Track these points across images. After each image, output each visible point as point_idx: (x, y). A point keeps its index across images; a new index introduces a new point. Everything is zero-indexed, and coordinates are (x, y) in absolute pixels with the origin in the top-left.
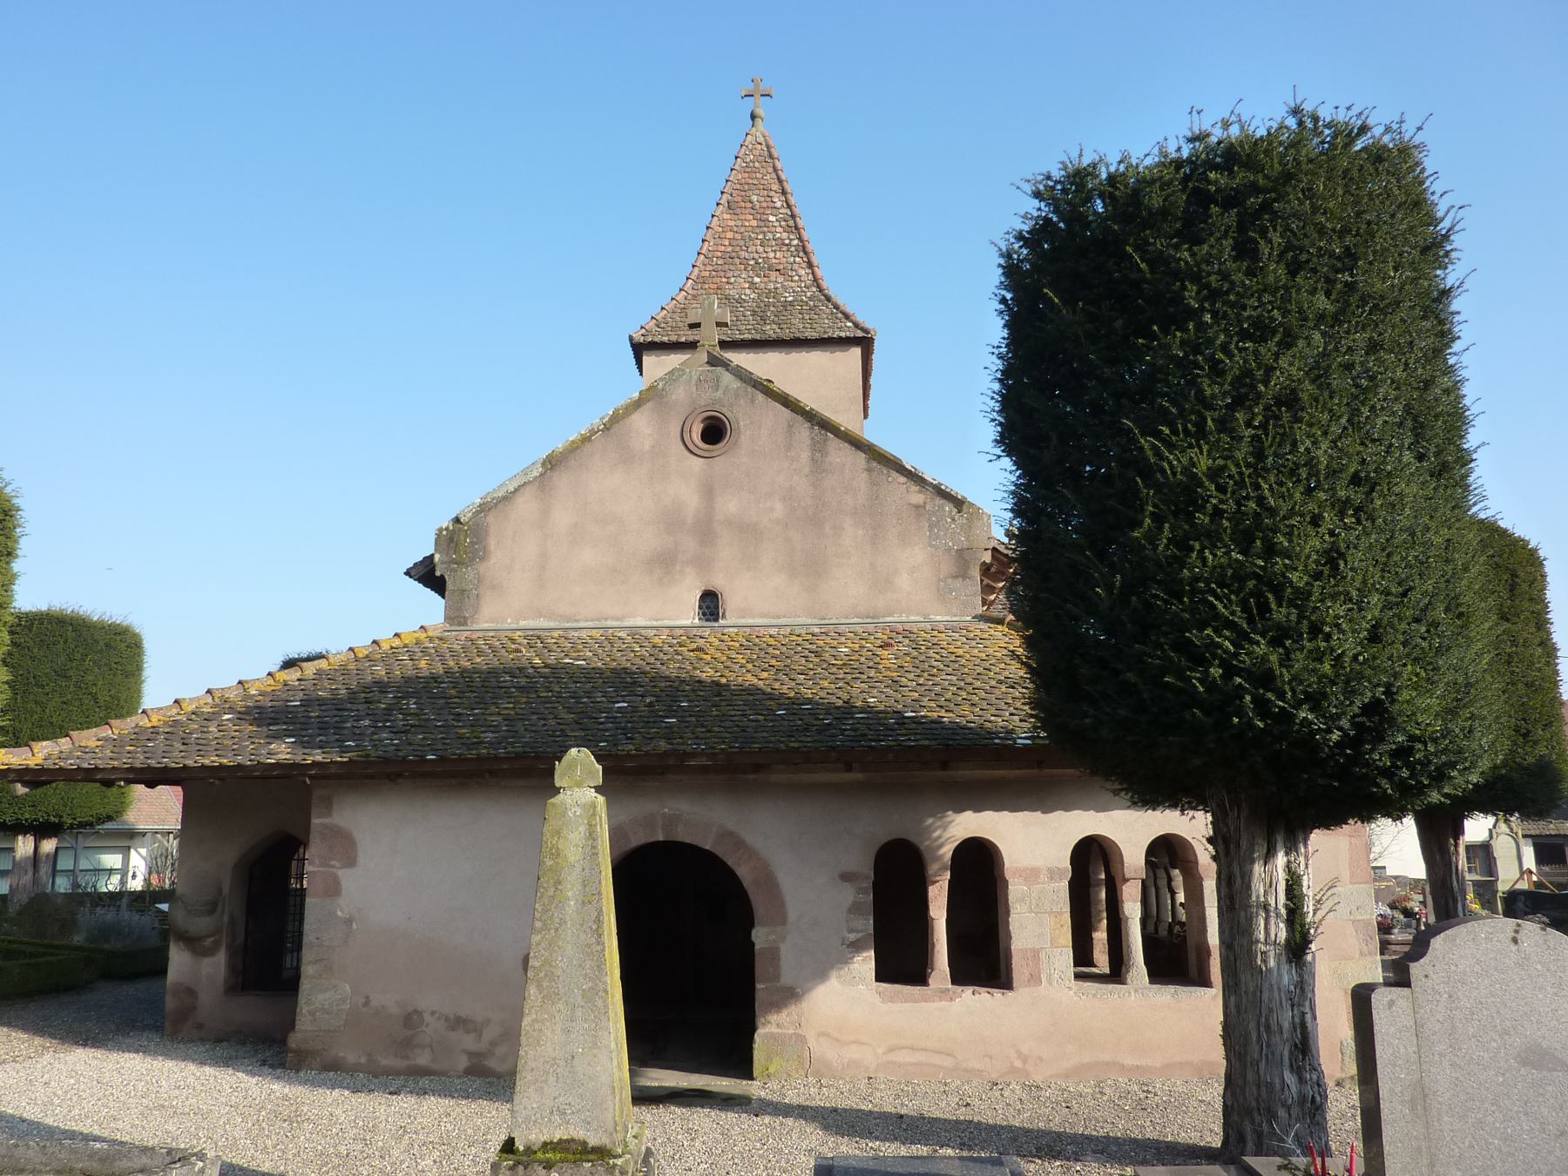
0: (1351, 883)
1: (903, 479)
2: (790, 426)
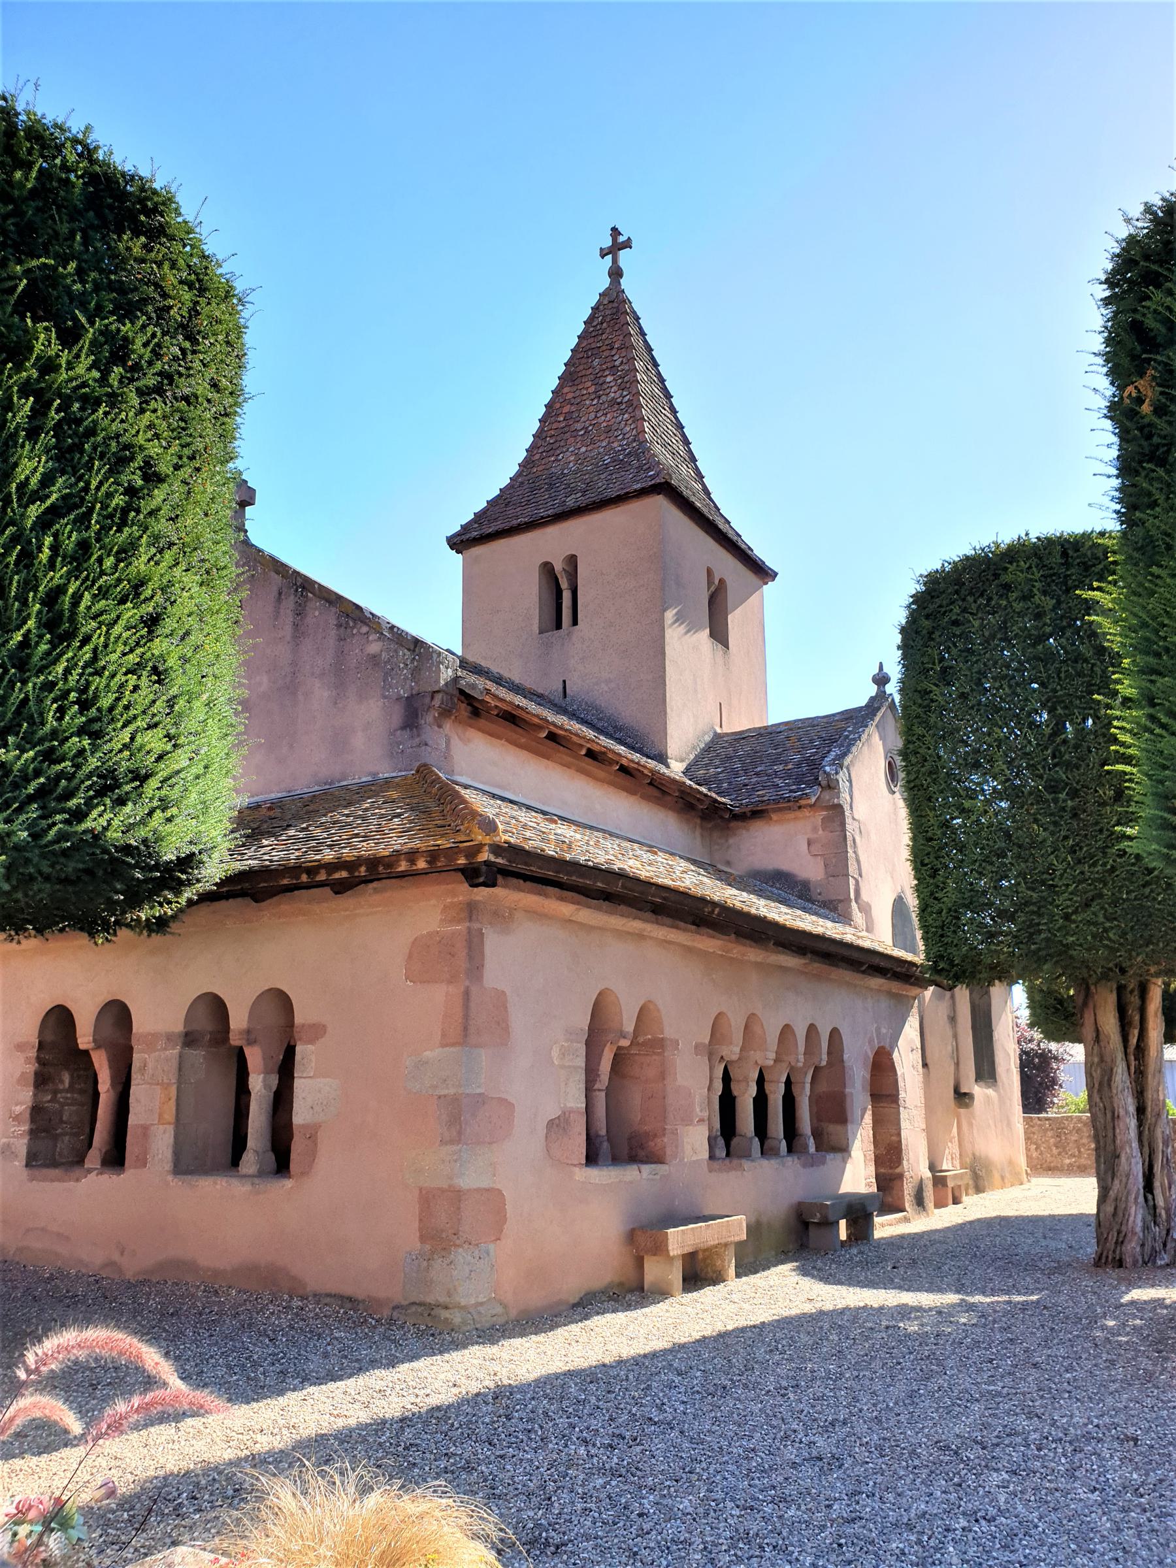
0: (443, 1045)
2: (280, 594)
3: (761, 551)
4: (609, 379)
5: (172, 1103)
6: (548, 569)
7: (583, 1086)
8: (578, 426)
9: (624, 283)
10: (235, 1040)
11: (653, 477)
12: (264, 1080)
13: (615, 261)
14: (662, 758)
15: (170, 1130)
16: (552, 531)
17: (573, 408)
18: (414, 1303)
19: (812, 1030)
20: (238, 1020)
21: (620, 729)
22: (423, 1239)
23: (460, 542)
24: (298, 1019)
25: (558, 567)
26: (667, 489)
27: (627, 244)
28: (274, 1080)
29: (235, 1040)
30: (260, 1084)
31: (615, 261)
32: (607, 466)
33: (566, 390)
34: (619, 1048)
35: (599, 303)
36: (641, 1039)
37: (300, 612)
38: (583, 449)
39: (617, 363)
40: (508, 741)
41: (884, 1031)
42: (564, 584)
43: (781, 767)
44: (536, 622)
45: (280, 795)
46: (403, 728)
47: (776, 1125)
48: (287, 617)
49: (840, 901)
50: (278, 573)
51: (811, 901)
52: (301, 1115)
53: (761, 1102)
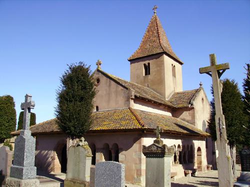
3: (182, 62)
19: (188, 146)
47: (182, 160)
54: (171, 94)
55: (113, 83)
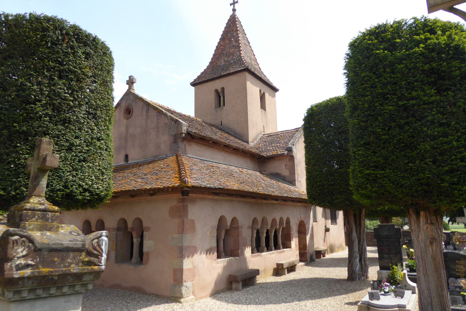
1: (164, 116)
2: (143, 107)
3: (275, 84)
4: (233, 39)
5: (114, 246)
6: (217, 91)
7: (216, 240)
8: (225, 52)
9: (237, 13)
10: (129, 230)
11: (244, 67)
12: (137, 240)
13: (234, 7)
14: (247, 142)
15: (114, 252)
16: (218, 81)
17: (223, 47)
18: (172, 297)
19: (281, 220)
20: (130, 225)
21: (237, 134)
22: (174, 281)
23: (193, 84)
24: (144, 225)
25: (220, 90)
26: (247, 70)
27: (237, 2)
28: (139, 240)
29: (129, 230)
30: (136, 241)
31: (234, 7)
32: (232, 63)
33: (221, 42)
34: (226, 229)
35: (230, 19)
36: (233, 226)
37: (147, 111)
38: (226, 59)
39: (235, 35)
40: (202, 144)
41: (302, 216)
42: (221, 95)
43: (279, 144)
44: (214, 107)
45: (144, 160)
46: (173, 143)
48: (145, 113)
49: (293, 181)
50: (142, 101)
51: (285, 181)
52: (145, 250)
53: (267, 238)
54: (258, 136)
55: (152, 113)
